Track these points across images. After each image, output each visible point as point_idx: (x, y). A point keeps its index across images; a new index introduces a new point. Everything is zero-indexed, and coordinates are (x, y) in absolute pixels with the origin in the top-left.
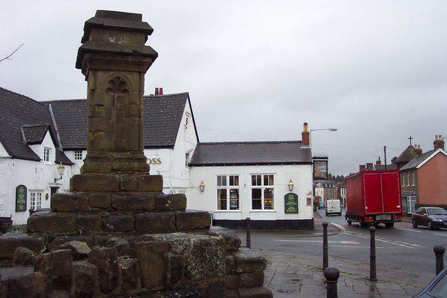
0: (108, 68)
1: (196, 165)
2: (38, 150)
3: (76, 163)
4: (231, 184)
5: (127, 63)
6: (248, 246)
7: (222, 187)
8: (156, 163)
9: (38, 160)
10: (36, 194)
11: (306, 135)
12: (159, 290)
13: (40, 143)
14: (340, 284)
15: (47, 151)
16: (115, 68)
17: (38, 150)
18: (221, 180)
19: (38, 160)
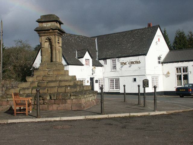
0: (44, 35)
1: (165, 63)
2: (83, 61)
3: (104, 65)
4: (184, 72)
5: (50, 32)
6: (139, 86)
7: (179, 74)
8: (138, 63)
9: (83, 65)
10: (101, 80)
11: (15, 41)
12: (69, 86)
13: (82, 57)
14: (126, 87)
15: (87, 60)
16: (43, 35)
17: (83, 61)
18: (178, 69)
19: (83, 65)
